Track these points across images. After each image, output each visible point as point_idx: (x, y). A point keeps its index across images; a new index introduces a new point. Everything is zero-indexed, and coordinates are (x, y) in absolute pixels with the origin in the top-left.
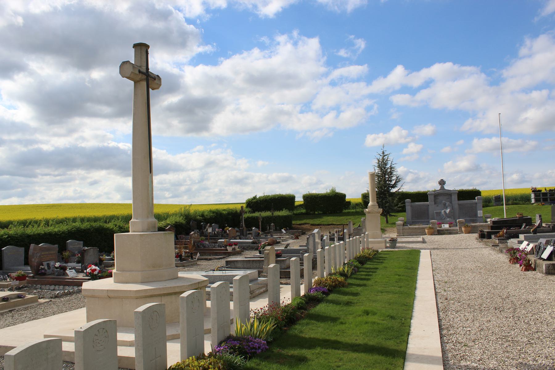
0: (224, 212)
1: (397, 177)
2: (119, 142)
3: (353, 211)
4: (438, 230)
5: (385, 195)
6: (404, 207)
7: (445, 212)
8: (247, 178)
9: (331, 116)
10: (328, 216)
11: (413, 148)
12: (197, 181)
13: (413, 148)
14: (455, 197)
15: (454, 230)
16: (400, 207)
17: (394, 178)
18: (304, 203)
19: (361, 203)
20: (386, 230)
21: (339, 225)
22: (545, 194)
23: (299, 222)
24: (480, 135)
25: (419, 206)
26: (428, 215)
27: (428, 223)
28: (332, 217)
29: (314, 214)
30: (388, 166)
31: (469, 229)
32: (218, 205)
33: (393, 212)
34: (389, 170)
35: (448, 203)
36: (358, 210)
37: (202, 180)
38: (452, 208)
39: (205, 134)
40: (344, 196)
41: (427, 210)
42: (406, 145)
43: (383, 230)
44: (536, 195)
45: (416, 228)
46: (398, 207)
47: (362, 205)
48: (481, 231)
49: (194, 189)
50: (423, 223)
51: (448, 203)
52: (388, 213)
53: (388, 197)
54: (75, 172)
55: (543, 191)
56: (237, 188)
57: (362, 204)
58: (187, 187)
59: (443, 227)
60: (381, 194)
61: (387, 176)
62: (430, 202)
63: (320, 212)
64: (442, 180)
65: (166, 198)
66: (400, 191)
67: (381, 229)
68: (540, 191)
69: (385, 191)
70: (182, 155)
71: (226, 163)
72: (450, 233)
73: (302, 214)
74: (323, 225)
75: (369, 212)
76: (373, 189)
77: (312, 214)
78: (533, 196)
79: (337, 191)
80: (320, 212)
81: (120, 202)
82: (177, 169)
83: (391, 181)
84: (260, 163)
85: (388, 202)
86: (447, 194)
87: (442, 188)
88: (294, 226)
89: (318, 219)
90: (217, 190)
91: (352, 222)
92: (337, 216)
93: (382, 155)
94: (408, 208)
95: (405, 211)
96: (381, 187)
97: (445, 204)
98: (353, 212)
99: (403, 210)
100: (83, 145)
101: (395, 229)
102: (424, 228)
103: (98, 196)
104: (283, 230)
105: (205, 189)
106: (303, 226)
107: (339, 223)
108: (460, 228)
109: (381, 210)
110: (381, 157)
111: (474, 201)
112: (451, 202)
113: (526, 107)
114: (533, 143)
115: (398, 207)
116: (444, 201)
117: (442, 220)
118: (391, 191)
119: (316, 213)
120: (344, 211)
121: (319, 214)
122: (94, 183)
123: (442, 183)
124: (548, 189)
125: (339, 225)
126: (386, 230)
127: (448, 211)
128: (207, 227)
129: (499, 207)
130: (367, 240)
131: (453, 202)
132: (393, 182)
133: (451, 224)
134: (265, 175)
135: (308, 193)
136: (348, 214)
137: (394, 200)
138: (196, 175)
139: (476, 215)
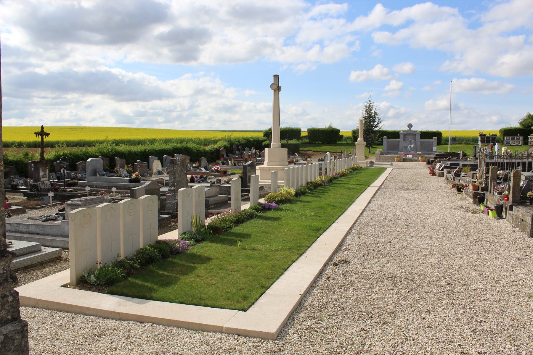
0: (252, 140)
1: (379, 120)
2: (111, 67)
3: (344, 142)
4: (403, 159)
5: (369, 132)
6: (382, 142)
7: (410, 147)
8: (235, 106)
9: (316, 48)
10: (326, 146)
11: (394, 85)
12: (187, 108)
13: (394, 85)
14: (418, 137)
15: (414, 159)
16: (379, 142)
17: (377, 120)
18: (308, 135)
19: (351, 137)
20: (368, 157)
21: (334, 152)
22: (488, 138)
23: (304, 149)
24: (460, 76)
25: (393, 141)
26: (399, 148)
27: (397, 154)
28: (329, 147)
29: (315, 143)
30: (373, 111)
31: (424, 159)
32: (227, 132)
33: (374, 145)
34: (373, 114)
35: (413, 141)
36: (348, 142)
37: (192, 107)
38: (416, 144)
39: (193, 63)
40: (338, 131)
41: (398, 145)
42: (388, 82)
43: (366, 157)
44: (482, 138)
45: (388, 157)
46: (378, 142)
47: (351, 139)
48: (428, 160)
49: (184, 116)
50: (394, 154)
51: (413, 141)
52: (371, 145)
53: (371, 133)
54: (70, 96)
55: (488, 135)
56: (226, 116)
57: (352, 137)
58: (178, 113)
59: (407, 157)
60: (366, 131)
61: (371, 119)
62: (401, 140)
63: (319, 142)
64: (410, 124)
65: (159, 123)
66: (380, 129)
67: (68, 249)
68: (485, 135)
69: (369, 129)
70: (172, 81)
71: (215, 92)
72: (411, 161)
73: (306, 143)
74: (322, 152)
75: (358, 144)
76: (361, 128)
77: (314, 144)
78: (479, 139)
79: (333, 127)
80: (319, 142)
81: (114, 126)
82: (169, 96)
83: (374, 122)
84: (248, 92)
85: (371, 138)
86: (413, 134)
87: (410, 130)
88: (300, 152)
89: (319, 148)
90: (206, 117)
91: (346, 150)
92: (333, 146)
93: (369, 103)
94: (385, 143)
95: (382, 145)
96: (367, 126)
97: (411, 141)
98: (344, 143)
99: (381, 144)
100: (76, 69)
101: (375, 157)
102: (394, 157)
103: (93, 120)
104: (296, 154)
105: (196, 115)
106: (307, 152)
107: (334, 151)
108: (418, 158)
109: (365, 143)
110: (369, 104)
111: (431, 140)
112: (415, 140)
113: (505, 51)
114: (510, 86)
115: (378, 142)
116: (410, 139)
117: (408, 152)
118: (374, 129)
119: (317, 143)
120: (338, 142)
121: (319, 144)
122: (89, 107)
123: (410, 126)
124: (491, 134)
125: (334, 152)
126: (368, 157)
127: (412, 146)
128: (252, 149)
129: (455, 145)
130: (356, 161)
131: (417, 140)
132: (375, 124)
133: (413, 155)
134: (253, 104)
135: (311, 127)
136: (341, 145)
137: (375, 136)
138: (186, 103)
139: (432, 150)
